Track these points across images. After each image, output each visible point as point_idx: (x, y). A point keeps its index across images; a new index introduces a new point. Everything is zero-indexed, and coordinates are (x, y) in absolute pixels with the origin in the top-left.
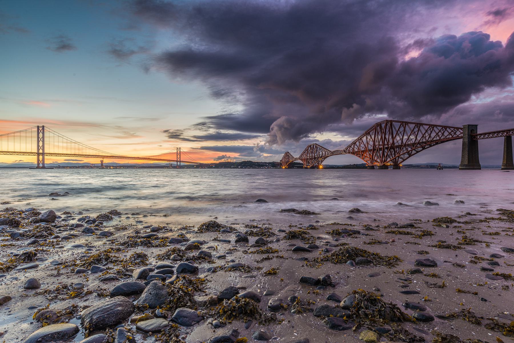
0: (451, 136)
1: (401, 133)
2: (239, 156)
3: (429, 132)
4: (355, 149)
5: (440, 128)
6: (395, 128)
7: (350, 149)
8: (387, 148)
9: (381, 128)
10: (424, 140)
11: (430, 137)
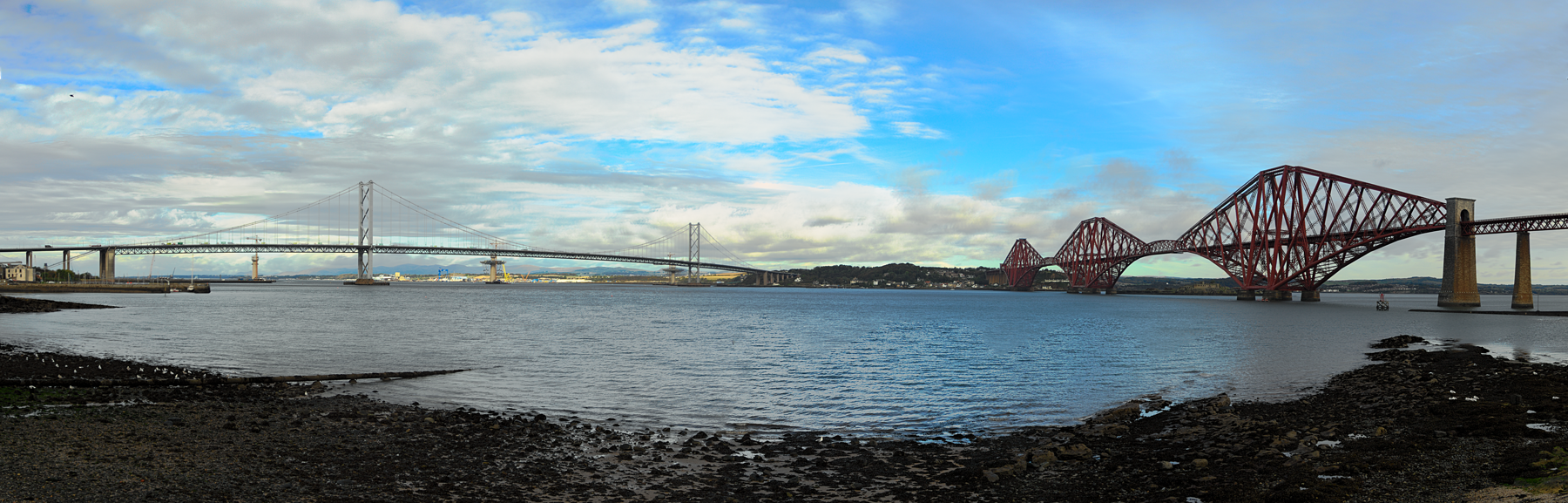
0: (1423, 223)
1: (1319, 202)
2: (452, 260)
3: (1382, 207)
4: (1208, 239)
5: (1403, 199)
6: (1307, 190)
7: (1194, 238)
8: (1287, 242)
9: (1273, 184)
10: (1370, 228)
11: (1383, 219)
